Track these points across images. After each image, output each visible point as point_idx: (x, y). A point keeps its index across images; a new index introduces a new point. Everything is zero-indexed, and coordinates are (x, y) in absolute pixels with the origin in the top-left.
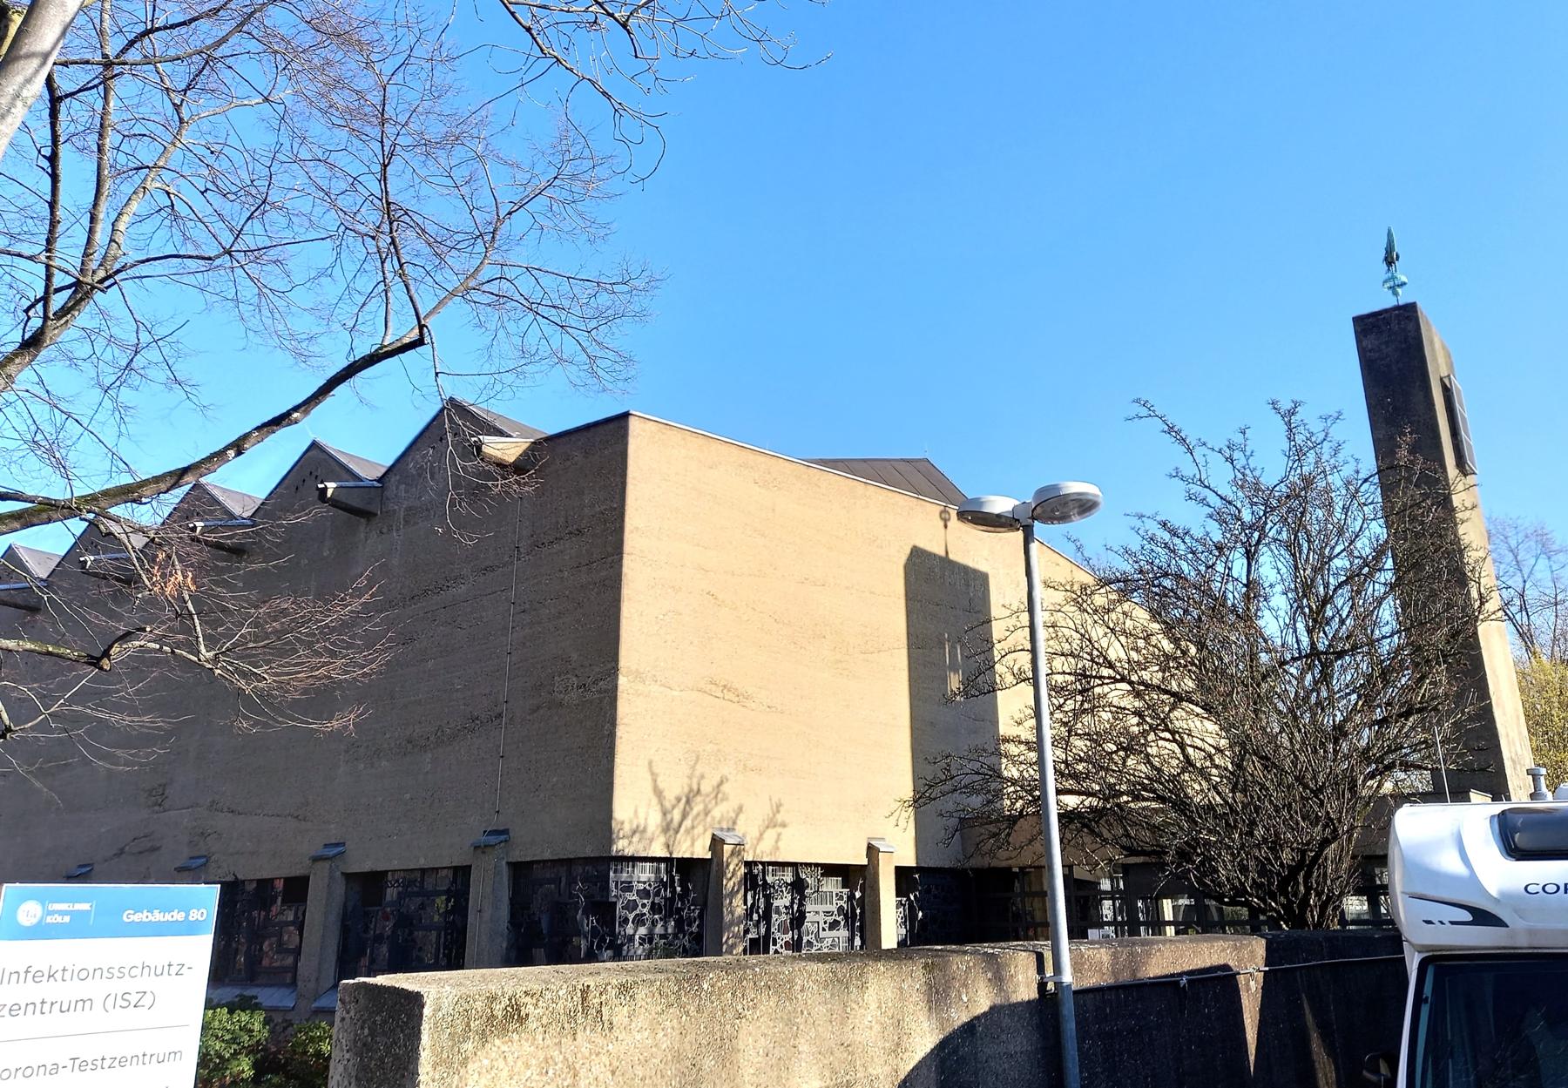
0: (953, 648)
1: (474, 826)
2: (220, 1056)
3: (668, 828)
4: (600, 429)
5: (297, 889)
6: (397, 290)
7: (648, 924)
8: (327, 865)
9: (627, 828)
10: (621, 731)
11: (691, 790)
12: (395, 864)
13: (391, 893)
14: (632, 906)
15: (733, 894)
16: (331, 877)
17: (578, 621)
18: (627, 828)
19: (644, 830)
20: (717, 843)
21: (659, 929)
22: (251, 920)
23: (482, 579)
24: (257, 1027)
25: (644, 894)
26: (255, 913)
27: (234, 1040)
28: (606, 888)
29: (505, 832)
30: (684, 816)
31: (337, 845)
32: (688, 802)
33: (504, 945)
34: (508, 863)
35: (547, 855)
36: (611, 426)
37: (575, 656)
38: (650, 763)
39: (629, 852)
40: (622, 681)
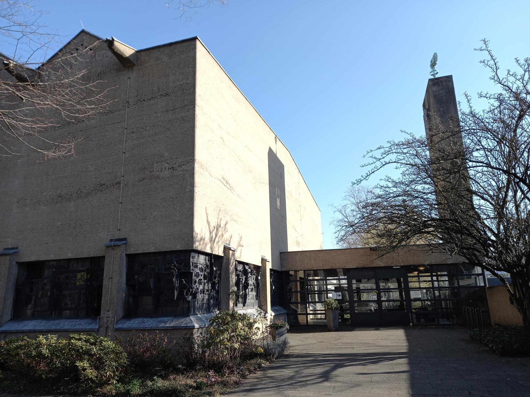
1: (105, 236)
3: (212, 241)
4: (178, 45)
7: (203, 284)
8: (8, 258)
9: (199, 237)
10: (196, 190)
11: (218, 225)
12: (52, 257)
13: (47, 272)
14: (197, 275)
15: (232, 272)
18: (199, 237)
19: (204, 240)
20: (226, 249)
21: (206, 287)
25: (201, 270)
29: (125, 239)
30: (216, 235)
31: (13, 249)
32: (217, 230)
33: (124, 295)
34: (126, 255)
35: (152, 250)
36: (186, 44)
37: (166, 154)
39: (199, 248)
40: (196, 166)
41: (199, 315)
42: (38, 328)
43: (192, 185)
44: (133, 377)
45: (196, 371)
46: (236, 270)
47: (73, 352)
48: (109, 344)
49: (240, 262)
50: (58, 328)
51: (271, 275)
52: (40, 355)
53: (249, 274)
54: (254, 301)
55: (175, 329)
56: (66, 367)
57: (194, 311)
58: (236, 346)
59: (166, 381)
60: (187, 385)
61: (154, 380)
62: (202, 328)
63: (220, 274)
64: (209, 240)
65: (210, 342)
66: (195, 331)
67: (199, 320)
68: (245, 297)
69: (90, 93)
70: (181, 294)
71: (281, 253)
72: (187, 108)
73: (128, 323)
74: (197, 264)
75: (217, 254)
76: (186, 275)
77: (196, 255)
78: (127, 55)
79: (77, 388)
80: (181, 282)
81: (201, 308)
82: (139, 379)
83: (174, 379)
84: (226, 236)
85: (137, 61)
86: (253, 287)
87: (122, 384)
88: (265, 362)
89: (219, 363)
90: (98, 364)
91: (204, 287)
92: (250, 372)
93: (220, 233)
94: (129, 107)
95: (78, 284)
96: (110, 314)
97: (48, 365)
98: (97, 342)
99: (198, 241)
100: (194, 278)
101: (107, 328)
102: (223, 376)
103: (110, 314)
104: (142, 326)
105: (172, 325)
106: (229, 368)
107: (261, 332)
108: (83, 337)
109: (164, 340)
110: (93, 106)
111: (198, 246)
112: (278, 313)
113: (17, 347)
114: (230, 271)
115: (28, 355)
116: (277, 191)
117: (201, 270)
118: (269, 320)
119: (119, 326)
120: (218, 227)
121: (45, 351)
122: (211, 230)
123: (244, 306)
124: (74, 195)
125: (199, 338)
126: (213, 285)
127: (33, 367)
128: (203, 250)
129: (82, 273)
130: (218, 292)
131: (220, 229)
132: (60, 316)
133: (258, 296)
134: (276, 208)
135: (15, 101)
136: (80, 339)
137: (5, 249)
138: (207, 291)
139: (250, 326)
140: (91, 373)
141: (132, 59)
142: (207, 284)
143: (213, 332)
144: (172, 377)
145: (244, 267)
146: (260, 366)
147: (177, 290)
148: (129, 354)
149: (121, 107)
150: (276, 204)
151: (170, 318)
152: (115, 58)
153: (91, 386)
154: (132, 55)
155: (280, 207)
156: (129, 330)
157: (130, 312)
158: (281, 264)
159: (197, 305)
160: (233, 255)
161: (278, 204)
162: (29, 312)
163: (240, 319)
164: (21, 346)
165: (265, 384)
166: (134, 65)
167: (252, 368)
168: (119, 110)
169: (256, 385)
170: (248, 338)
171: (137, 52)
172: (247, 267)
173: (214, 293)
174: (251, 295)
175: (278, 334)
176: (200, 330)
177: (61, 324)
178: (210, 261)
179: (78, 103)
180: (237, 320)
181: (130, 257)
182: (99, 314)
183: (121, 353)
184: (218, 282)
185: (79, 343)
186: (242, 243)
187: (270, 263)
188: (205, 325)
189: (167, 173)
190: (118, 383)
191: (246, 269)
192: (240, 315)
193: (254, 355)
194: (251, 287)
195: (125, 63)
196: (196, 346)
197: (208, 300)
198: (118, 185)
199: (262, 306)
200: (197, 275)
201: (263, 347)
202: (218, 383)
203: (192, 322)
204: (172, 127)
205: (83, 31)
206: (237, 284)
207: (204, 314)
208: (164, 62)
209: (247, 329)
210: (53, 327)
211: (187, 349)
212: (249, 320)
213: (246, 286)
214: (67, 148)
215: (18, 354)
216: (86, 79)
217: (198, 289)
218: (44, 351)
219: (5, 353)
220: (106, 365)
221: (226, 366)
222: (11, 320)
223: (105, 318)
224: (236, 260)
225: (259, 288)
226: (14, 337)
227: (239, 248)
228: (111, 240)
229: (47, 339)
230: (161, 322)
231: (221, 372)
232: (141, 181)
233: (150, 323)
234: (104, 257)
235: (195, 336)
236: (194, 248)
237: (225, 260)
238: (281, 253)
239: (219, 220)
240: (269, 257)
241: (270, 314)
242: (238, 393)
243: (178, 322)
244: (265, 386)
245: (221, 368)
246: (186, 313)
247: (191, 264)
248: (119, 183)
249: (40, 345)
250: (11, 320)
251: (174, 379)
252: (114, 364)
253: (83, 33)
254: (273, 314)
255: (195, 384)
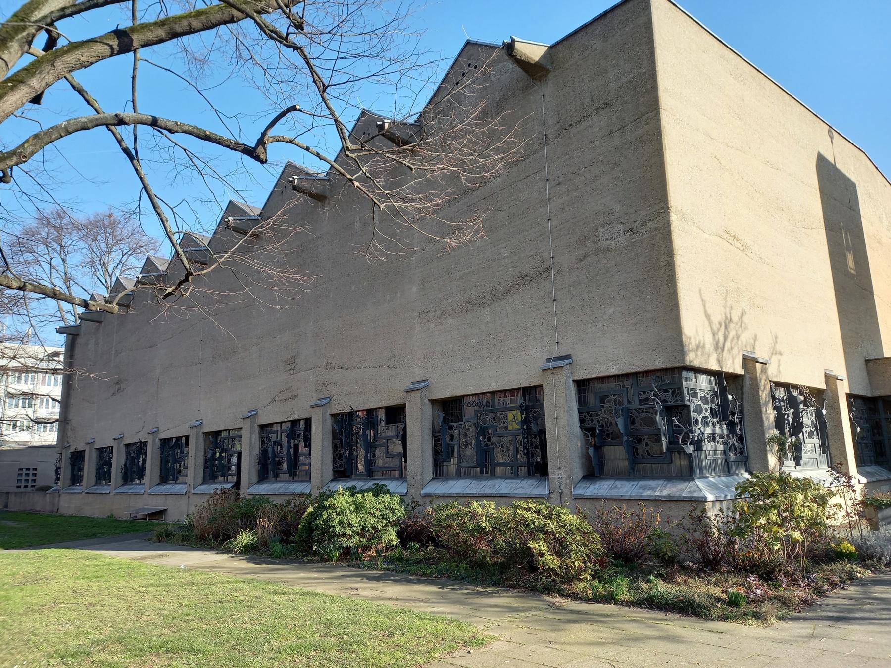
0: (846, 234)
2: (374, 528)
3: (719, 348)
5: (396, 414)
6: (386, 71)
7: (711, 424)
8: (418, 394)
10: (679, 261)
11: (726, 317)
12: (472, 390)
13: (469, 413)
14: (699, 410)
15: (766, 404)
16: (422, 403)
17: (617, 178)
19: (704, 347)
20: (749, 361)
21: (718, 431)
22: (365, 436)
23: (515, 169)
24: (397, 506)
25: (705, 400)
26: (368, 432)
27: (383, 517)
28: (681, 394)
30: (725, 338)
31: (422, 381)
32: (726, 327)
33: (579, 445)
34: (574, 381)
35: (614, 371)
37: (617, 208)
38: (700, 291)
39: (697, 363)
40: (674, 217)
41: (711, 479)
42: (467, 491)
43: (670, 253)
44: (615, 572)
45: (722, 573)
46: (774, 398)
47: (522, 528)
48: (570, 517)
49: (779, 384)
50: (493, 491)
51: (850, 406)
52: (479, 529)
53: (802, 406)
54: (817, 456)
55: (670, 500)
56: (515, 549)
57: (701, 471)
58: (797, 535)
59: (671, 586)
60: (710, 596)
61: (649, 581)
62: (720, 501)
63: (741, 406)
64: (713, 348)
65: (741, 526)
66: (709, 505)
67: (713, 487)
68: (797, 448)
69: (493, 135)
70: (672, 442)
71: (867, 362)
72: (644, 118)
73: (592, 487)
74: (695, 390)
75: (731, 371)
76: (678, 410)
77: (692, 375)
78: (537, 59)
79: (536, 580)
80: (670, 422)
81: (713, 466)
82: (625, 577)
83: (685, 583)
84: (745, 337)
85: (553, 63)
86: (813, 430)
87: (600, 581)
88: (862, 570)
89: (765, 565)
90: (560, 548)
91: (714, 431)
92: (833, 585)
93: (732, 333)
94: (548, 144)
95: (510, 428)
96: (562, 473)
97: (490, 543)
98: (552, 514)
99: (692, 350)
100: (693, 414)
101: (561, 494)
102: (777, 587)
103: (562, 473)
104: (615, 493)
105: (665, 493)
106: (786, 574)
107: (844, 512)
108: (532, 506)
109: (655, 517)
110: (502, 155)
111: (693, 359)
112: (874, 479)
113: (449, 517)
114: (762, 401)
115: (465, 530)
116: (846, 238)
117: (705, 400)
118: (859, 492)
119: (579, 492)
120: (727, 323)
121: (485, 524)
122: (715, 328)
123: (798, 463)
124: (488, 297)
125: (718, 519)
126: (731, 425)
127: (472, 545)
128: (705, 366)
129: (514, 412)
130: (741, 439)
131: (732, 326)
132: (493, 475)
133: (824, 447)
134: (846, 273)
135: (398, 173)
136: (528, 509)
137: (413, 383)
138: (721, 436)
139: (821, 501)
140: (551, 560)
141: (543, 63)
142: (718, 426)
143: (746, 508)
144: (680, 580)
145: (789, 392)
146: (852, 578)
147: (665, 435)
148: (603, 536)
149: (536, 147)
150: (846, 264)
151: (661, 482)
152: (518, 69)
153: (554, 581)
154: (544, 57)
155: (855, 270)
156: (597, 499)
157: (594, 471)
158: (871, 383)
159: (706, 463)
160: (764, 371)
161: (851, 263)
162: (453, 469)
163: (798, 487)
164: (452, 515)
165: (871, 611)
166: (548, 71)
167: (836, 579)
168: (534, 153)
169: (850, 611)
170: (819, 523)
171: (551, 48)
172: (795, 393)
173: (733, 441)
174: (811, 445)
175: (883, 519)
176: (718, 505)
177: (497, 487)
178: (719, 383)
179: (481, 156)
180: (794, 490)
181: (582, 385)
182: (548, 474)
183: (591, 533)
184: (740, 422)
185: (528, 514)
186: (778, 347)
187: (846, 383)
188: (726, 496)
189: (622, 240)
190: (594, 579)
191: (792, 397)
192: (798, 480)
193: (835, 556)
194: (808, 430)
195: (534, 72)
196: (715, 530)
197: (725, 453)
198: (547, 274)
199: (837, 466)
200: (699, 410)
201: (853, 542)
202: (770, 599)
203: (701, 490)
204: (622, 159)
205: (468, 43)
206: (779, 423)
207: (719, 477)
208: (596, 50)
209: (814, 506)
210: (487, 491)
211: (698, 535)
212: (818, 489)
213: (797, 427)
214: (473, 227)
215: (450, 526)
216: (484, 115)
217: (703, 434)
218: (483, 524)
219: (434, 523)
220: (572, 550)
221: (780, 571)
222: (433, 479)
223: (556, 480)
224: (771, 381)
225: (825, 430)
226: (442, 502)
227: (775, 359)
228: (548, 360)
229: (483, 507)
230: (645, 488)
231: (771, 579)
232: (581, 260)
233: (626, 489)
234: (541, 386)
235: (711, 514)
236: (688, 363)
237: (748, 382)
238: (867, 362)
239: (728, 310)
240: (840, 370)
241: (859, 481)
242: (816, 622)
243: (674, 490)
244: (872, 615)
245: (772, 571)
246: (688, 474)
247: (685, 391)
248: (548, 269)
249: (474, 515)
250: (433, 479)
251: (685, 583)
252: (582, 549)
253: (468, 46)
254: (864, 480)
255: (724, 596)
